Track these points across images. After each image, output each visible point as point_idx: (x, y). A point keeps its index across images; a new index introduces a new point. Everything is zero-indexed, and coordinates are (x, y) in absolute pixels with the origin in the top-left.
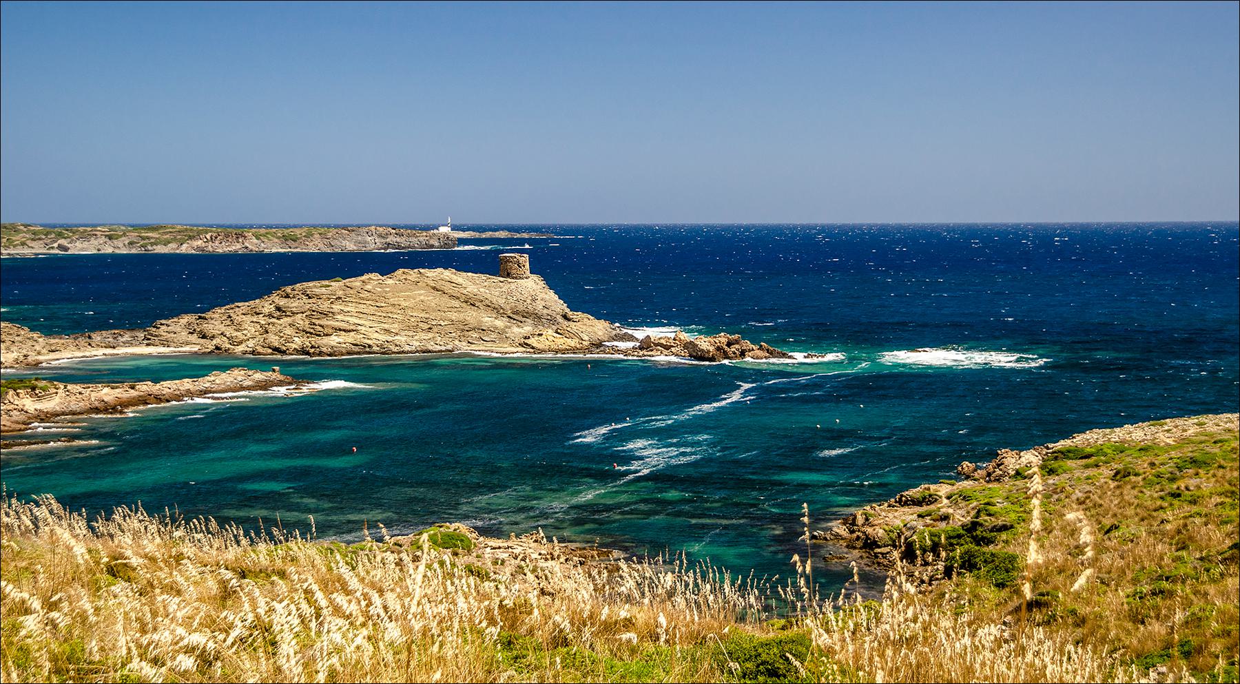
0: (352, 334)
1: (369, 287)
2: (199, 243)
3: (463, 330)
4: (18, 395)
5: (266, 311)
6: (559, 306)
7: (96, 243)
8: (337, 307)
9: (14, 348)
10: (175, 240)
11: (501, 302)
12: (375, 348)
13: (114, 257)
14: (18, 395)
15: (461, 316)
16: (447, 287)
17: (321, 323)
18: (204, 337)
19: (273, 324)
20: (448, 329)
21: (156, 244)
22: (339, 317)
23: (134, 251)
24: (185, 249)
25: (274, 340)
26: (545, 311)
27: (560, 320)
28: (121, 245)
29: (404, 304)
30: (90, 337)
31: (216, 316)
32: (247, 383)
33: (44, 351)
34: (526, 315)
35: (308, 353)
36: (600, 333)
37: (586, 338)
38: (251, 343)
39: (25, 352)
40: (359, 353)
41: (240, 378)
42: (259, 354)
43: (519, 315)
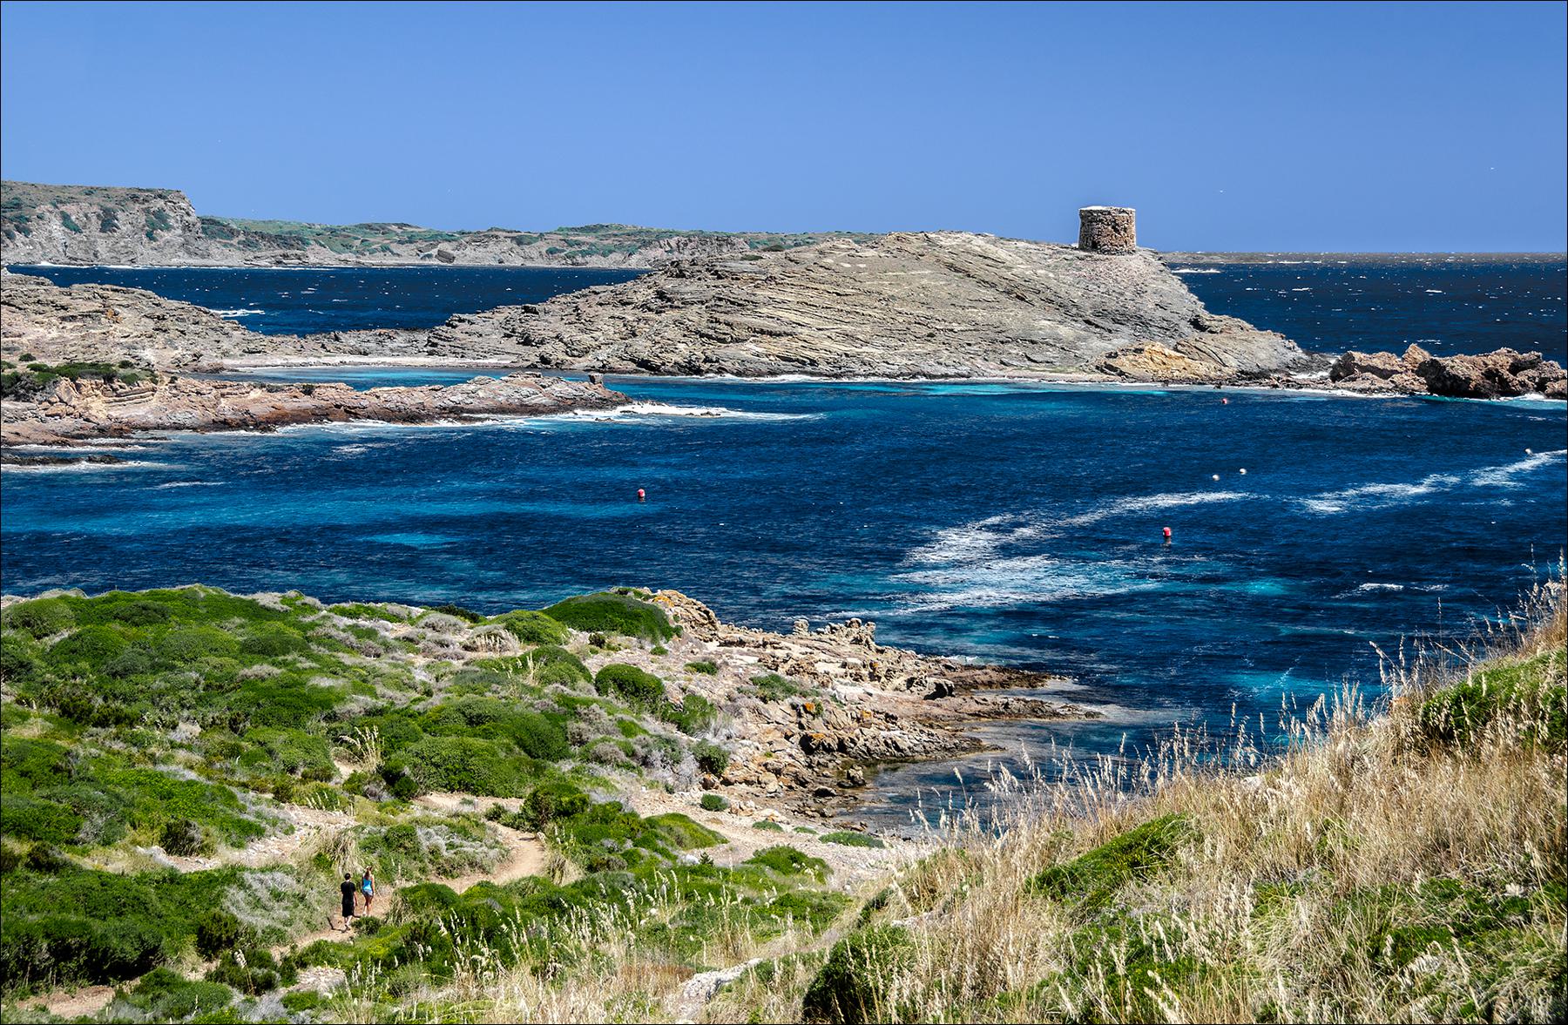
0: (784, 340)
1: (829, 261)
4: (78, 387)
5: (639, 298)
7: (497, 249)
8: (763, 294)
9: (181, 342)
10: (620, 247)
11: (1076, 294)
12: (823, 367)
14: (78, 387)
15: (994, 317)
16: (976, 266)
17: (729, 318)
18: (527, 342)
19: (647, 320)
20: (965, 338)
22: (764, 310)
23: (555, 265)
25: (642, 348)
26: (1160, 313)
27: (1186, 328)
28: (535, 254)
29: (888, 291)
30: (337, 339)
31: (556, 307)
32: (540, 400)
33: (237, 351)
34: (1121, 318)
36: (1262, 355)
37: (1233, 362)
38: (603, 354)
39: (197, 349)
41: (525, 391)
42: (612, 370)
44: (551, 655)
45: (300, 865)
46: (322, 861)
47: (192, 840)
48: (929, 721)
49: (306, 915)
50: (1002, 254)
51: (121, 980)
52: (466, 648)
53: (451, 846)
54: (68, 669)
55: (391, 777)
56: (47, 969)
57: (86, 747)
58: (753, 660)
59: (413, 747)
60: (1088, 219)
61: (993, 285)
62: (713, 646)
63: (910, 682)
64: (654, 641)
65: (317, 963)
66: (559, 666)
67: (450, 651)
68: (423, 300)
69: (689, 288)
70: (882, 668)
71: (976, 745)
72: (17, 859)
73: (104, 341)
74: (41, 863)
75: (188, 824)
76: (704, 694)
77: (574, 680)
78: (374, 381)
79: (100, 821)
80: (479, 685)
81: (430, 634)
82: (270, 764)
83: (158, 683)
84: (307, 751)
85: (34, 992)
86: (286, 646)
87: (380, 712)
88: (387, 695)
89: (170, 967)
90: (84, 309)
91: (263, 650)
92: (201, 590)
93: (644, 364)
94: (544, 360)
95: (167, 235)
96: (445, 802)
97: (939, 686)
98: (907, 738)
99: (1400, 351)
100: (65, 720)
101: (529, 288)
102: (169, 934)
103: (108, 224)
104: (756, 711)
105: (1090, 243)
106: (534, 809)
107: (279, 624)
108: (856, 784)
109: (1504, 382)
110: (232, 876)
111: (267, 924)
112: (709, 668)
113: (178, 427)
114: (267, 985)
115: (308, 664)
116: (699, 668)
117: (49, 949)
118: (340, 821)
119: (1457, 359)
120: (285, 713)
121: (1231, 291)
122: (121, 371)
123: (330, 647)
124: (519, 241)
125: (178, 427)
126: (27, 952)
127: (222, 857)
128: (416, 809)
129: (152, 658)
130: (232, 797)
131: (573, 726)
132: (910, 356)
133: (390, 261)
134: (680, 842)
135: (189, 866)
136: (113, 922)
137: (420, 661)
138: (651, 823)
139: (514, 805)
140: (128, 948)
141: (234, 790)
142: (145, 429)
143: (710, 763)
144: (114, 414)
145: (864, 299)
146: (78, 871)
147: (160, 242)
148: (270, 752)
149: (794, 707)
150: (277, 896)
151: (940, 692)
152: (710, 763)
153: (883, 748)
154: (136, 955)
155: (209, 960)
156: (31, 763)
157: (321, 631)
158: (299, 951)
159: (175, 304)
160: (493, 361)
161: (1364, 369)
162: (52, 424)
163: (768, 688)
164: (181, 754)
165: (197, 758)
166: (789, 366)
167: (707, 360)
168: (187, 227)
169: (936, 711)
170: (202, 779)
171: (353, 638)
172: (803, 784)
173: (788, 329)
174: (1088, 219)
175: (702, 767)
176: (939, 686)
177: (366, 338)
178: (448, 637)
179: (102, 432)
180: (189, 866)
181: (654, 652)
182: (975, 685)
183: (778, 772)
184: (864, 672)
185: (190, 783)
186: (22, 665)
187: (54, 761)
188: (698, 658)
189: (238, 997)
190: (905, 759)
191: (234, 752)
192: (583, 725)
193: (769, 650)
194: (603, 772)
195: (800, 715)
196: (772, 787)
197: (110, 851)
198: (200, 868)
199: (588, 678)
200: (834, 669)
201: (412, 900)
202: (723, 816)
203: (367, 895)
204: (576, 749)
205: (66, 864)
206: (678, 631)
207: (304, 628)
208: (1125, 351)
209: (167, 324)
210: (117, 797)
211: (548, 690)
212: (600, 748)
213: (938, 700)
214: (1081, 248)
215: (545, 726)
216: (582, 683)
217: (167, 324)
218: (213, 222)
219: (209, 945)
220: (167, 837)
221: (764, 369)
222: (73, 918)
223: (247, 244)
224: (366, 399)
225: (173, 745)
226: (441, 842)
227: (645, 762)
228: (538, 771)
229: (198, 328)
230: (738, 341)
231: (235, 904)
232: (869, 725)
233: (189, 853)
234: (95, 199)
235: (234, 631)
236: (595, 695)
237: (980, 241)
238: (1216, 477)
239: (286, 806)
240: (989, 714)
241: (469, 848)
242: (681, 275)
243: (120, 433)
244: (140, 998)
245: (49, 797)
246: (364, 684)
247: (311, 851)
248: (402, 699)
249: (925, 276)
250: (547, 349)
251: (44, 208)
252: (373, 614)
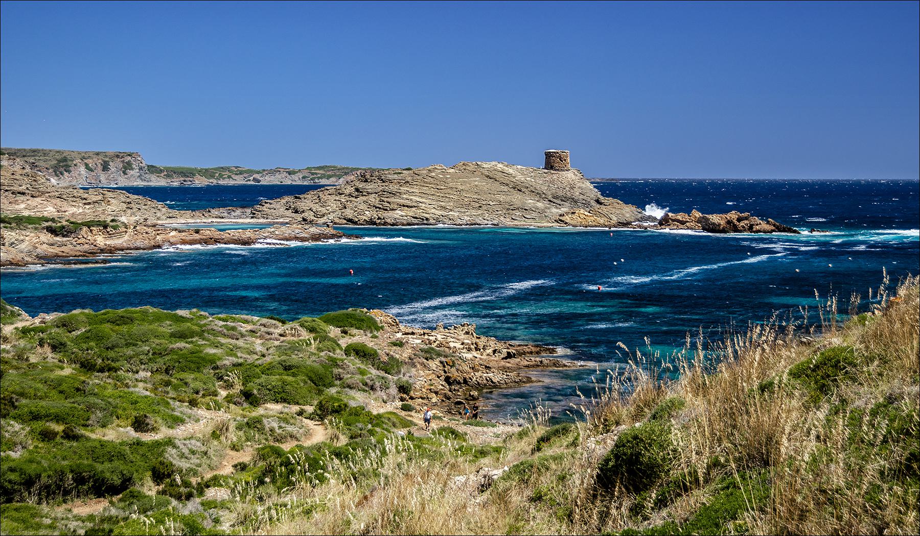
0: (414, 209)
3: (508, 209)
4: (91, 231)
5: (347, 192)
8: (403, 189)
14: (91, 231)
15: (508, 199)
16: (499, 176)
17: (389, 200)
18: (296, 212)
19: (351, 201)
20: (496, 208)
23: (305, 183)
25: (349, 213)
27: (593, 203)
28: (297, 179)
29: (460, 187)
33: (164, 217)
34: (565, 199)
35: (375, 224)
38: (331, 217)
40: (418, 224)
41: (297, 231)
42: (335, 223)
44: (323, 338)
45: (204, 436)
46: (215, 435)
47: (148, 424)
48: (505, 369)
49: (208, 462)
50: (511, 171)
51: (111, 496)
52: (281, 335)
53: (280, 427)
54: (85, 346)
55: (247, 395)
56: (71, 490)
57: (95, 380)
58: (420, 341)
59: (257, 381)
60: (548, 155)
61: (507, 185)
62: (399, 335)
63: (494, 352)
64: (371, 332)
65: (215, 485)
66: (327, 343)
67: (273, 336)
68: (248, 197)
69: (370, 187)
70: (481, 345)
71: (529, 380)
72: (56, 434)
73: (103, 213)
74: (69, 435)
75: (146, 416)
76: (398, 356)
77: (334, 350)
78: (230, 227)
79: (99, 414)
80: (289, 352)
81: (263, 329)
82: (186, 389)
83: (129, 352)
84: (205, 384)
85: (65, 502)
86: (192, 334)
87: (240, 365)
88: (241, 357)
89: (137, 488)
90: (95, 199)
91: (181, 336)
92: (151, 309)
93: (350, 221)
94: (304, 220)
95: (132, 172)
96: (275, 408)
97: (508, 353)
98: (497, 377)
99: (689, 212)
100: (82, 369)
101: (297, 191)
102: (137, 471)
103: (105, 167)
104: (422, 364)
105: (549, 166)
106: (320, 409)
107: (189, 324)
108: (474, 398)
109: (735, 226)
110: (170, 442)
111: (188, 465)
112: (400, 344)
113: (137, 249)
114: (189, 496)
115: (204, 342)
116: (395, 344)
117: (73, 479)
118: (221, 416)
119: (714, 216)
120: (193, 366)
121: (609, 189)
122: (111, 224)
123: (214, 335)
125: (137, 249)
126: (61, 480)
127: (163, 433)
128: (260, 411)
129: (126, 340)
130: (168, 403)
131: (336, 371)
132: (471, 216)
133: (231, 183)
134: (394, 426)
135: (147, 438)
136: (107, 465)
137: (259, 341)
138: (379, 416)
139: (310, 409)
140: (115, 478)
141: (169, 400)
142: (122, 250)
143: (404, 389)
144: (108, 243)
145: (449, 191)
146: (88, 439)
147: (129, 175)
148: (186, 384)
149: (441, 362)
150: (193, 452)
151: (509, 356)
152: (404, 389)
153: (485, 382)
154: (119, 482)
155: (158, 485)
156: (64, 387)
157: (209, 327)
158: (205, 479)
159: (136, 197)
160: (281, 220)
161: (673, 220)
162: (78, 248)
163: (429, 353)
164: (141, 385)
165: (149, 386)
166: (416, 221)
167: (379, 218)
168: (141, 169)
169: (508, 365)
170: (153, 395)
171: (225, 331)
172: (449, 398)
173: (415, 204)
174: (548, 155)
175: (400, 391)
176: (508, 353)
177: (223, 211)
178: (272, 330)
179: (102, 251)
180: (147, 438)
181: (372, 337)
182: (524, 353)
183: (436, 393)
184: (472, 347)
185: (146, 397)
186: (61, 344)
187: (76, 385)
188: (393, 339)
189: (174, 502)
190: (495, 387)
191: (168, 383)
192: (340, 370)
193: (426, 337)
194: (352, 393)
195: (444, 366)
196: (434, 400)
197: (106, 430)
198: (152, 438)
199: (341, 349)
200: (458, 345)
201: (262, 455)
202: (413, 413)
204: (338, 382)
205: (82, 436)
206: (382, 328)
207: (201, 326)
208: (567, 213)
209: (132, 205)
210: (109, 403)
211: (322, 354)
212: (349, 381)
213: (508, 360)
214: (545, 168)
215: (321, 370)
216: (338, 351)
217: (132, 205)
218: (152, 166)
219: (158, 477)
220: (135, 423)
221: (405, 222)
222: (86, 462)
223: (168, 176)
224: (225, 235)
225: (137, 380)
226: (275, 425)
227: (372, 388)
228: (320, 392)
229: (146, 207)
230: (393, 210)
231: (171, 455)
232: (478, 371)
233: (146, 431)
234: (100, 157)
235: (167, 327)
236: (345, 357)
237: (500, 165)
239: (195, 409)
240: (533, 366)
241: (290, 428)
242: (366, 181)
243: (111, 252)
244: (122, 504)
245: (74, 403)
246: (231, 352)
247: (210, 429)
248: (251, 358)
249: (477, 181)
250: (305, 215)
251: (78, 161)
252: (234, 320)
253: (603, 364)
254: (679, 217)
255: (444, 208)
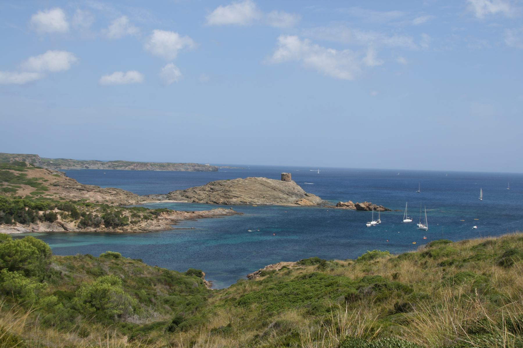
2: (132, 167)
6: (302, 191)
13: (103, 171)
16: (265, 183)
21: (117, 167)
24: (127, 169)
27: (304, 196)
43: (291, 194)
124: (102, 164)
203: (224, 305)
238: (475, 227)
253: (108, 231)
254: (346, 204)
255: (251, 198)
